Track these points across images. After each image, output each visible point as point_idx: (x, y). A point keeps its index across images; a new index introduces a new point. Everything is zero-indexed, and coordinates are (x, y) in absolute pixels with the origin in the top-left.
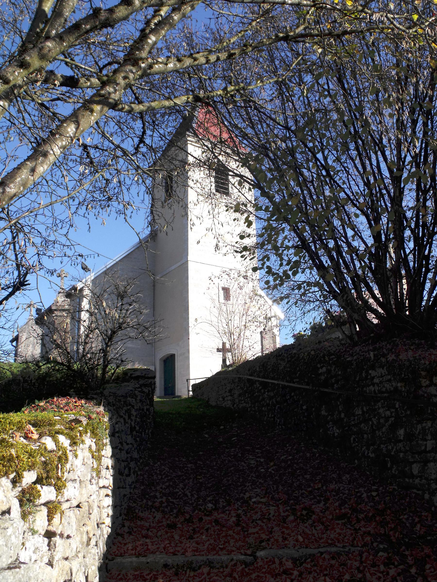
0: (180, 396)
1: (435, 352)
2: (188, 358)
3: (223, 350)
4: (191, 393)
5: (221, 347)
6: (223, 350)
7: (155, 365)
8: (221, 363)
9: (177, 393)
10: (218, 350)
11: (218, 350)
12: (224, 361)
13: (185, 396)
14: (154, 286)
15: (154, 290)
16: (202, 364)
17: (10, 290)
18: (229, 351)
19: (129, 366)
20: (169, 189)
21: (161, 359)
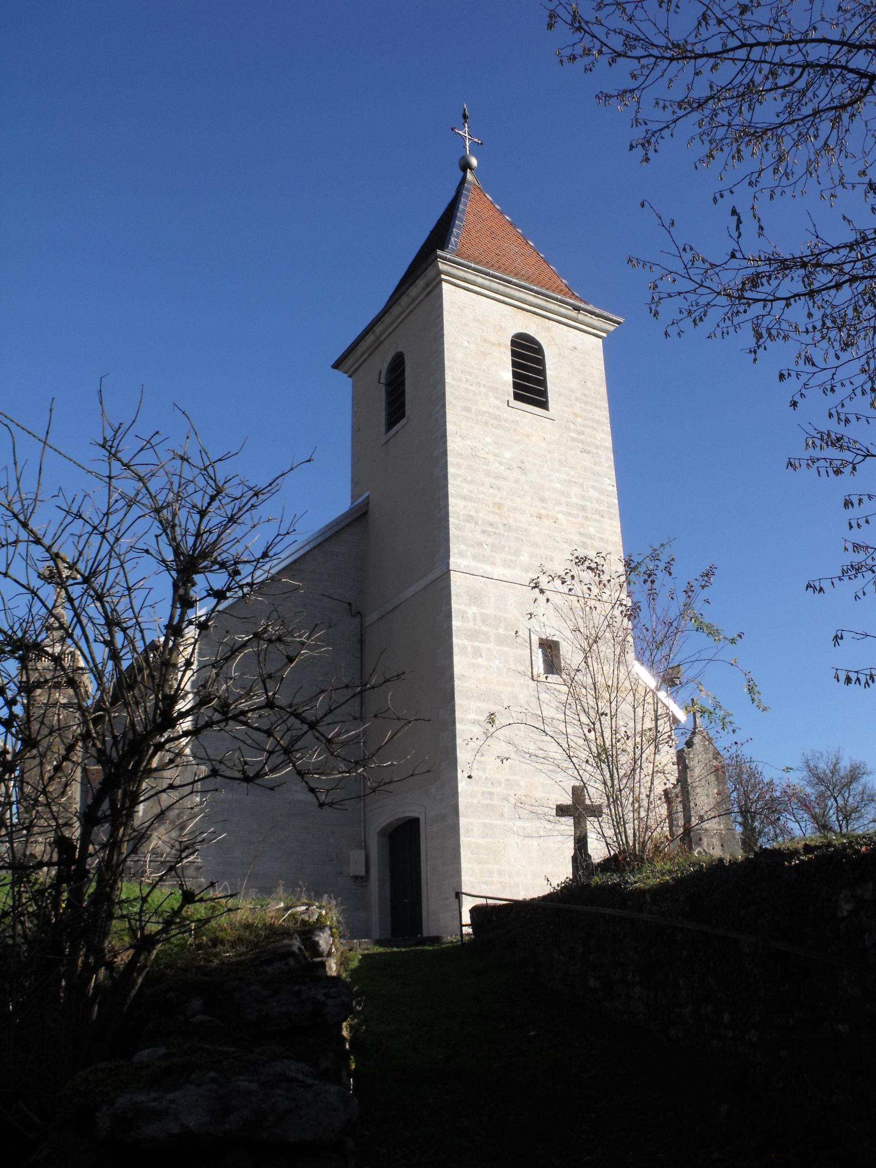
0: (436, 940)
1: (2, 799)
2: (454, 830)
3: (577, 810)
4: (467, 930)
5: (567, 800)
6: (577, 810)
7: (366, 848)
8: (569, 848)
9: (429, 929)
10: (562, 811)
11: (562, 811)
12: (581, 843)
13: (450, 938)
14: (361, 641)
15: (362, 651)
16: (508, 851)
17: (24, 672)
18: (596, 811)
19: (497, 647)
20: (396, 410)
21: (382, 833)
